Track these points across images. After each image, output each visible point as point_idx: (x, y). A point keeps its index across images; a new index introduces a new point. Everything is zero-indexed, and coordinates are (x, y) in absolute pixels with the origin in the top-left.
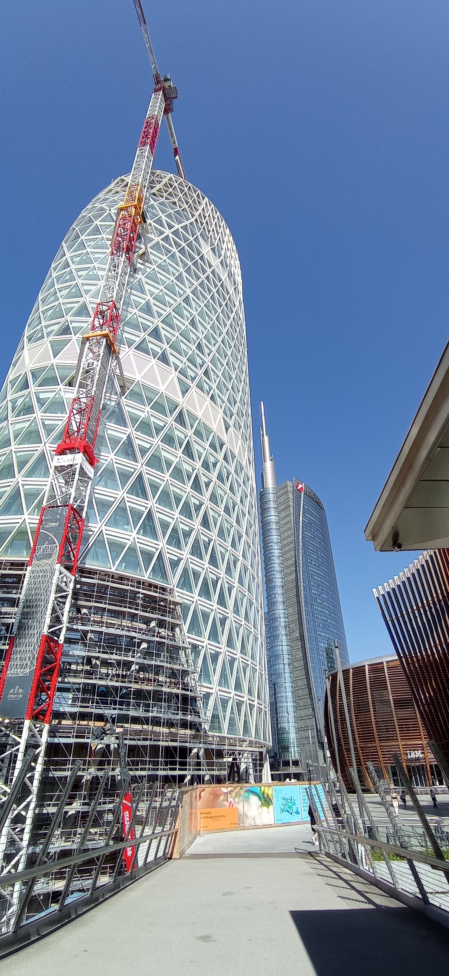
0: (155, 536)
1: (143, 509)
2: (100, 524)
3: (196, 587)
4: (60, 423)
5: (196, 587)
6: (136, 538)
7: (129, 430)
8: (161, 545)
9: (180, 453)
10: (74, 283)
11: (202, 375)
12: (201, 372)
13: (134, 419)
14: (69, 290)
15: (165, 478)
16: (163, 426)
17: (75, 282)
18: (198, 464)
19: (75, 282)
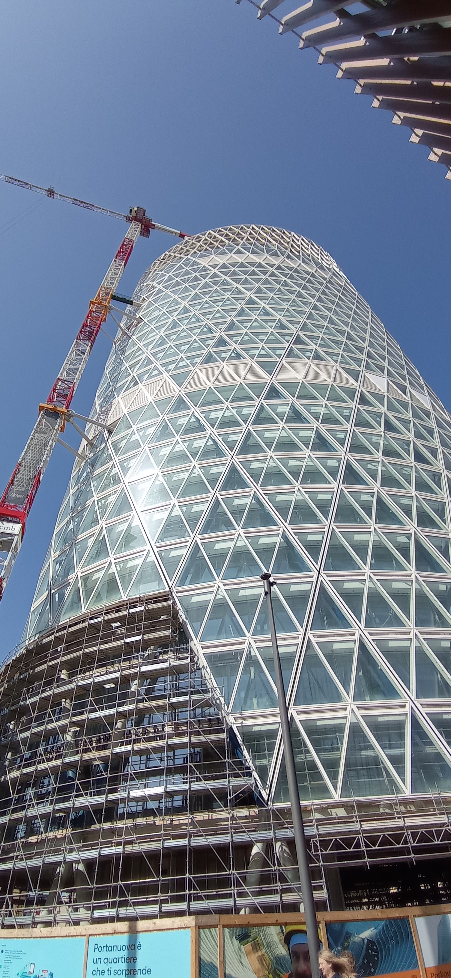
0: (389, 692)
1: (351, 645)
2: (302, 631)
3: (422, 444)
4: (183, 552)
5: (422, 444)
6: (356, 710)
7: (281, 527)
8: (409, 705)
9: (372, 523)
10: (152, 366)
11: (366, 359)
12: (364, 357)
13: (283, 509)
14: (175, 365)
15: (366, 577)
16: (343, 437)
17: (154, 365)
18: (412, 526)
19: (154, 365)
